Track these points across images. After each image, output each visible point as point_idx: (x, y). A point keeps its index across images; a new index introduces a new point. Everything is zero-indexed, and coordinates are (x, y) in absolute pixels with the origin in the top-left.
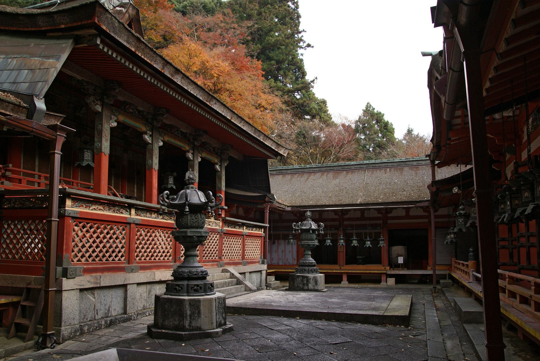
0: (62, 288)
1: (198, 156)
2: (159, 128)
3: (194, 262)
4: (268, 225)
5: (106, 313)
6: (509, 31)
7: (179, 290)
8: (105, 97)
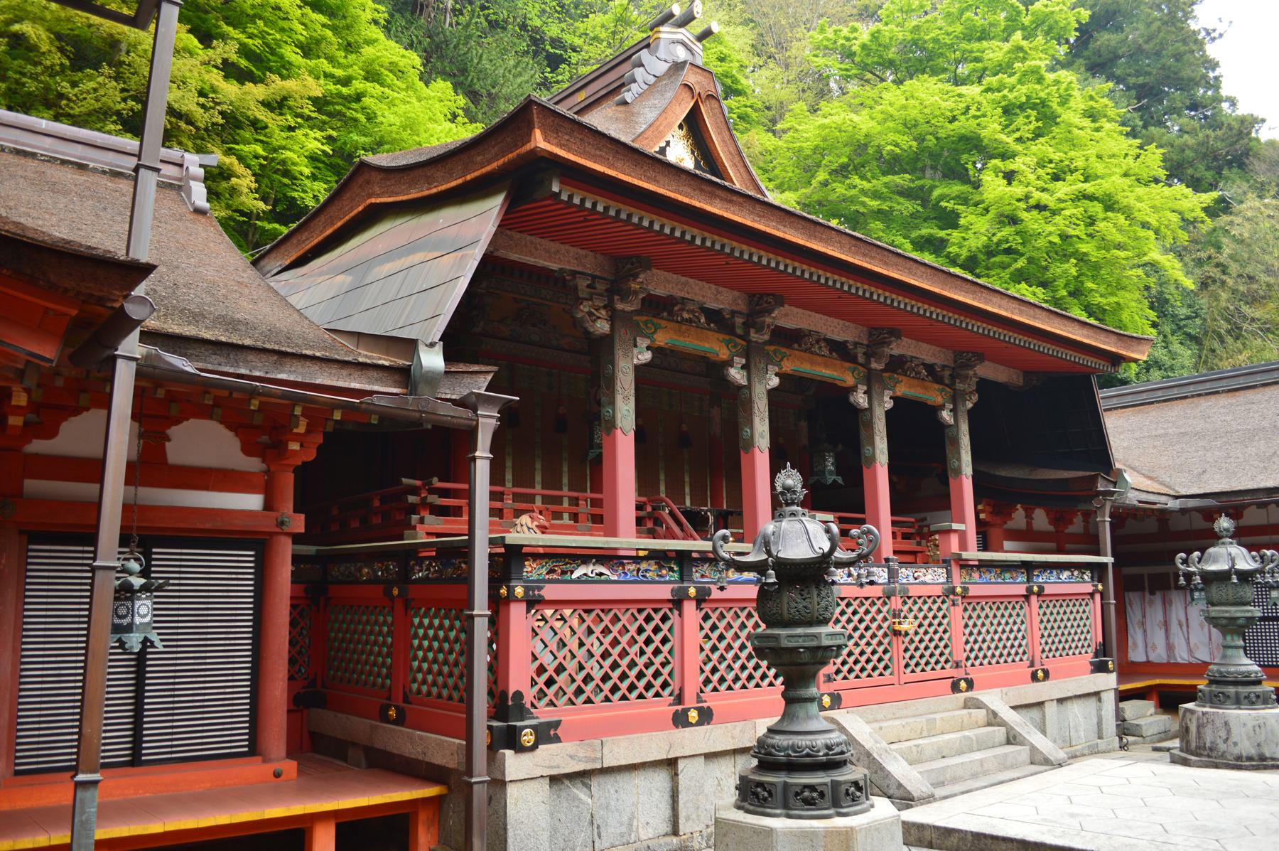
0: (503, 774)
1: (882, 395)
3: (809, 717)
5: (622, 835)
7: (765, 799)
8: (616, 297)
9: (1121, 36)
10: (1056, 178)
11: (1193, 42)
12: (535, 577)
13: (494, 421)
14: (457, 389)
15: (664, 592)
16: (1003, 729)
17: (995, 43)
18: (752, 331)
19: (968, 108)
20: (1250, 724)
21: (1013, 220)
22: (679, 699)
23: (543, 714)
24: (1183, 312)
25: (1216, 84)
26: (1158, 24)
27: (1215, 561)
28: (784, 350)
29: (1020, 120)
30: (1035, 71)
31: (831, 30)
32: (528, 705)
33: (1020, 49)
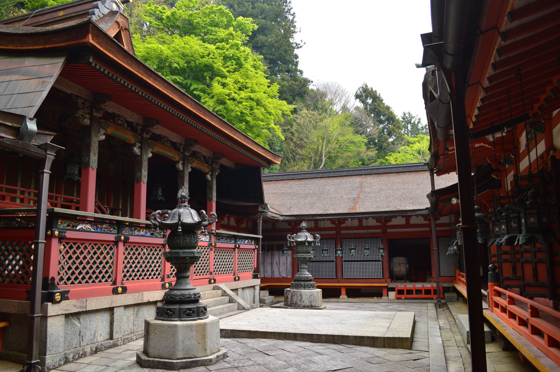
0: (46, 313)
2: (149, 139)
3: (186, 284)
4: (261, 237)
5: (91, 340)
6: (490, 71)
7: (171, 315)
8: (94, 110)
9: (266, 38)
10: (240, 89)
11: (290, 48)
12: (62, 228)
13: (53, 157)
14: (38, 140)
15: (112, 237)
16: (228, 297)
17: (221, 29)
18: (144, 133)
19: (209, 54)
20: (308, 295)
21: (223, 103)
22: (115, 283)
23: (62, 287)
24: (278, 148)
25: (296, 64)
26: (280, 37)
27: (300, 238)
28: (155, 142)
29: (229, 63)
30: (237, 45)
31: (153, 6)
32: (56, 284)
33: (232, 34)
